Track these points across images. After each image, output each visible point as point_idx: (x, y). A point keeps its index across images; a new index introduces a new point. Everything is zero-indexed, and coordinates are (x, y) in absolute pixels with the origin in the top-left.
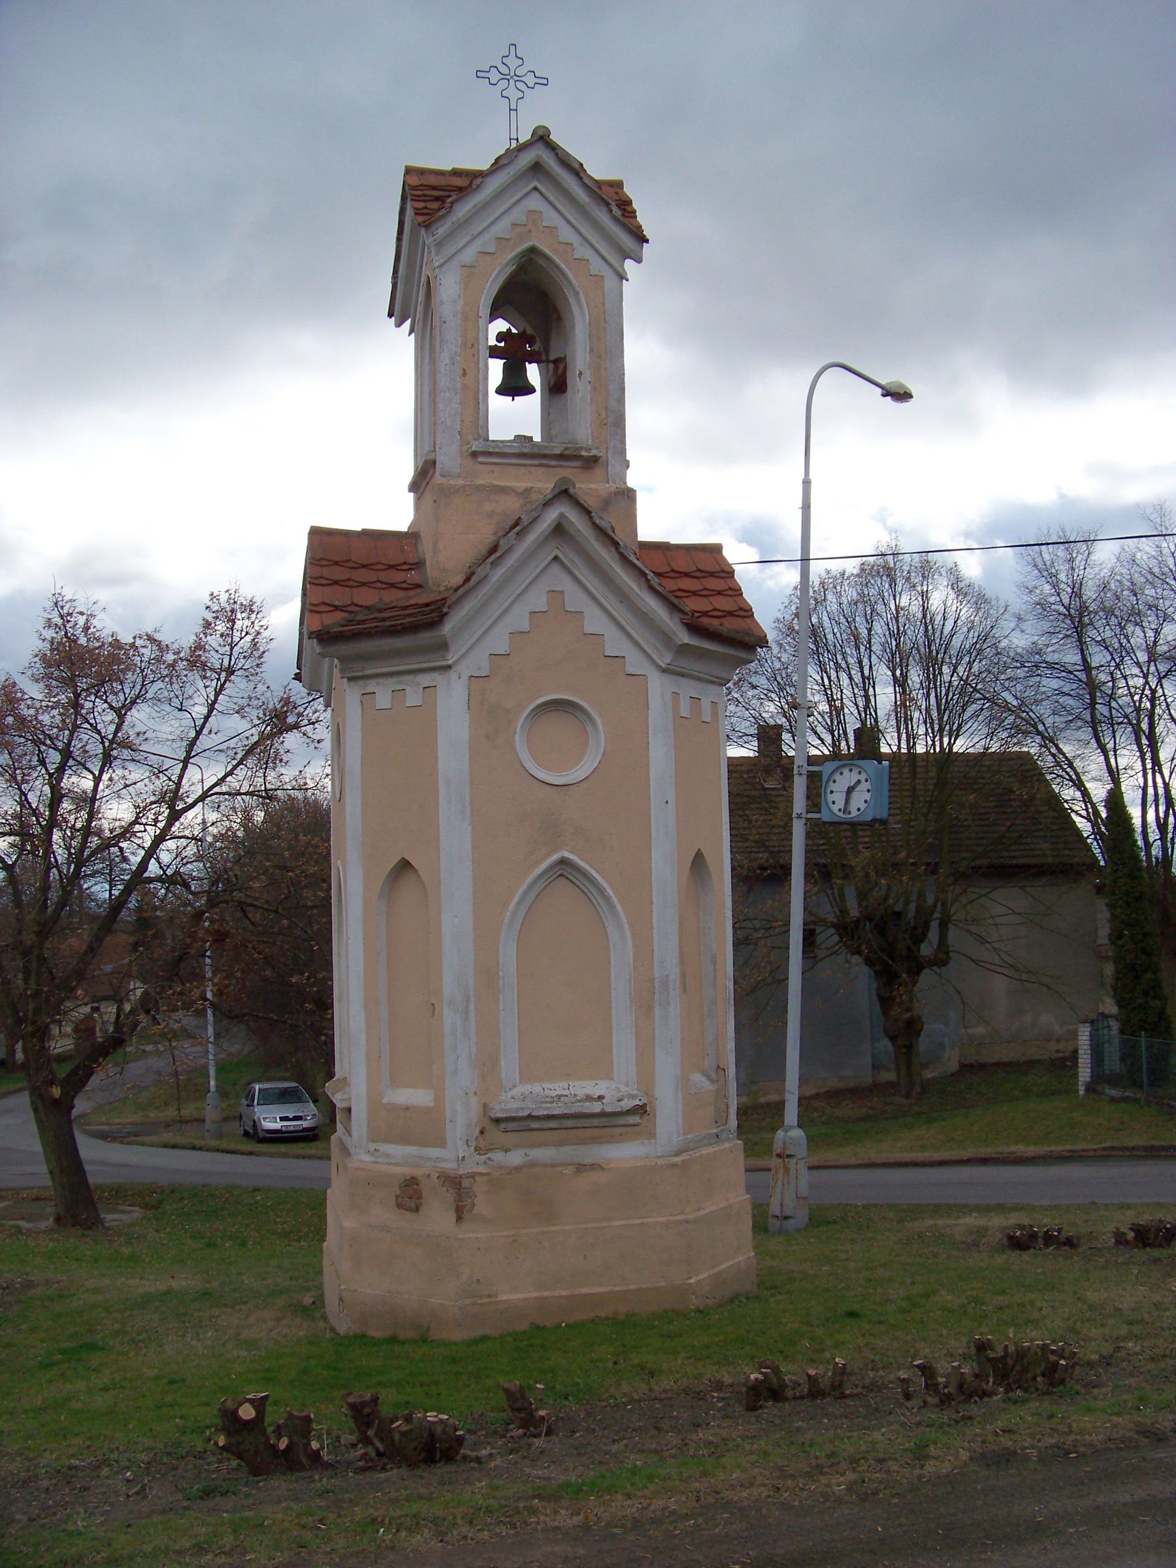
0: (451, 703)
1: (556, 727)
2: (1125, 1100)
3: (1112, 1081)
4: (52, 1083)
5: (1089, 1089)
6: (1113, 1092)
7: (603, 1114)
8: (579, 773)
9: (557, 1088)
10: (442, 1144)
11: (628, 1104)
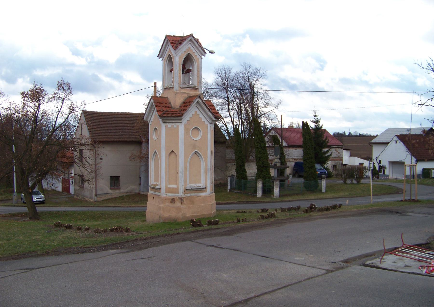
0: (181, 128)
1: (195, 131)
2: (238, 193)
3: (235, 189)
4: (29, 189)
5: (230, 190)
6: (236, 191)
7: (201, 189)
8: (198, 138)
9: (194, 185)
10: (178, 193)
11: (204, 187)
